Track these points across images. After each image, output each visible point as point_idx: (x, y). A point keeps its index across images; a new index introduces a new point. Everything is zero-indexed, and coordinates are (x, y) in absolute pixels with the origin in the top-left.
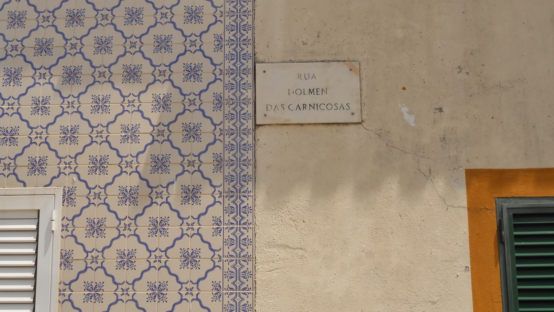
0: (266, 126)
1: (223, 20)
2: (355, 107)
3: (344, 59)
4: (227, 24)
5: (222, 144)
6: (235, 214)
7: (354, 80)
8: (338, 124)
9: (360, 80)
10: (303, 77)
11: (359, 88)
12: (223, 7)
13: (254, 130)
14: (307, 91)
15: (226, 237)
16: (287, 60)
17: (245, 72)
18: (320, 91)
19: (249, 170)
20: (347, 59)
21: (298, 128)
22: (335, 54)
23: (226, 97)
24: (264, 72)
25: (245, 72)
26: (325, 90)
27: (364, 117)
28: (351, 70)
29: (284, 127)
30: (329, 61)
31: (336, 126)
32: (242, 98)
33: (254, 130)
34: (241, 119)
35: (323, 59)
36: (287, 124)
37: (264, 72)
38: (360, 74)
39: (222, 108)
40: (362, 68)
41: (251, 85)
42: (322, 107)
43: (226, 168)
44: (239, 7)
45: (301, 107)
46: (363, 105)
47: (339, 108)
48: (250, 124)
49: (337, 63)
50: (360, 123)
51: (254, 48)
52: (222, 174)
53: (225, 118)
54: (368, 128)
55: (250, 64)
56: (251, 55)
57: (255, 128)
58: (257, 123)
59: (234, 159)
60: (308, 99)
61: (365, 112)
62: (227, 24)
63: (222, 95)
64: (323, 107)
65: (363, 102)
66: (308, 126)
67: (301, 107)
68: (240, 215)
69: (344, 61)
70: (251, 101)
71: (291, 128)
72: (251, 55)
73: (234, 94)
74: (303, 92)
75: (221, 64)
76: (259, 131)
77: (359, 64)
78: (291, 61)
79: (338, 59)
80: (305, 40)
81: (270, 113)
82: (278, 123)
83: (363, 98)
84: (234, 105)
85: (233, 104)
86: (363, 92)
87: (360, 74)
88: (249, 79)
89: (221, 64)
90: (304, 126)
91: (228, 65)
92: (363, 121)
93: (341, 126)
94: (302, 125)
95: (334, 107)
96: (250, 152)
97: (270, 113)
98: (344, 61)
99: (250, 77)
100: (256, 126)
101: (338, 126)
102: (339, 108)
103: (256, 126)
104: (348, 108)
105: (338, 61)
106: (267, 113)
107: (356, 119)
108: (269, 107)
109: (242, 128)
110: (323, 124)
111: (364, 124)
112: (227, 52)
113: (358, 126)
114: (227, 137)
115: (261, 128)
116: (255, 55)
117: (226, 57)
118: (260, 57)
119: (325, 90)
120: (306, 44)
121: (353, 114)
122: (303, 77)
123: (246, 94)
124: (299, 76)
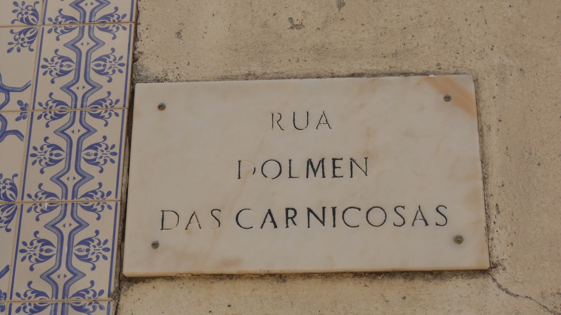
0: (158, 283)
1: (25, 132)
2: (465, 217)
3: (423, 68)
4: (37, 141)
5: (22, 145)
6: (61, 166)
7: (462, 136)
8: (408, 275)
9: (480, 130)
10: (287, 121)
11: (478, 155)
12: (29, 92)
13: (116, 295)
14: (299, 168)
15: (27, 236)
16: (236, 72)
17: (99, 109)
18: (344, 165)
19: (107, 178)
20: (434, 68)
21: (266, 289)
22: (395, 54)
23: (32, 189)
24: (161, 107)
25: (99, 109)
26: (362, 163)
27: (500, 252)
28: (447, 98)
29: (219, 286)
30: (374, 75)
31: (399, 283)
32: (74, 289)
33: (116, 295)
34: (83, 162)
35: (356, 68)
36: (231, 277)
37: (161, 107)
38: (479, 114)
39: (13, 225)
40: (485, 95)
41: (109, 245)
42: (351, 216)
43: (29, 218)
44: (76, 132)
45: (280, 217)
46: (494, 212)
47: (409, 220)
48: (100, 276)
49: (401, 78)
50: (484, 272)
51: (136, 39)
52: (33, 56)
53: (20, 256)
54: (513, 290)
55: (117, 87)
56: (124, 61)
57: (119, 289)
58: (128, 271)
59: (47, 289)
60: (305, 192)
61: (501, 237)
62: (37, 141)
63: (18, 182)
64: (352, 217)
65: (492, 202)
66: (302, 285)
67: (280, 217)
68: (78, 169)
69: (425, 74)
70: (112, 200)
71: (244, 287)
72: (124, 61)
73: (57, 179)
74: (285, 170)
75: (27, 87)
76: (132, 298)
77: (476, 81)
78: (248, 76)
79: (405, 68)
80: (298, 17)
81: (174, 238)
82: (196, 270)
83: (492, 188)
84: (56, 213)
85: (50, 209)
86: (494, 170)
87: (479, 114)
88: (111, 130)
89: (27, 87)
90: (289, 283)
91: (49, 89)
92: (494, 266)
93: (419, 283)
94: (281, 277)
95: (393, 218)
96: (111, 169)
97: (174, 238)
98: (425, 74)
99: (109, 217)
100: (124, 282)
101: (409, 284)
102: (409, 220)
103: (124, 282)
104: (442, 220)
105: (406, 74)
106: (163, 238)
107: (469, 257)
108: (170, 218)
109: (74, 289)
110: (357, 275)
111: (500, 276)
112: (48, 53)
113: (479, 281)
114: (39, 124)
115: (138, 290)
116: (135, 60)
117: (41, 66)
118: (150, 65)
119: (362, 163)
120: (299, 26)
121: (459, 240)
122: (287, 121)
123: (98, 178)
124: (276, 120)
